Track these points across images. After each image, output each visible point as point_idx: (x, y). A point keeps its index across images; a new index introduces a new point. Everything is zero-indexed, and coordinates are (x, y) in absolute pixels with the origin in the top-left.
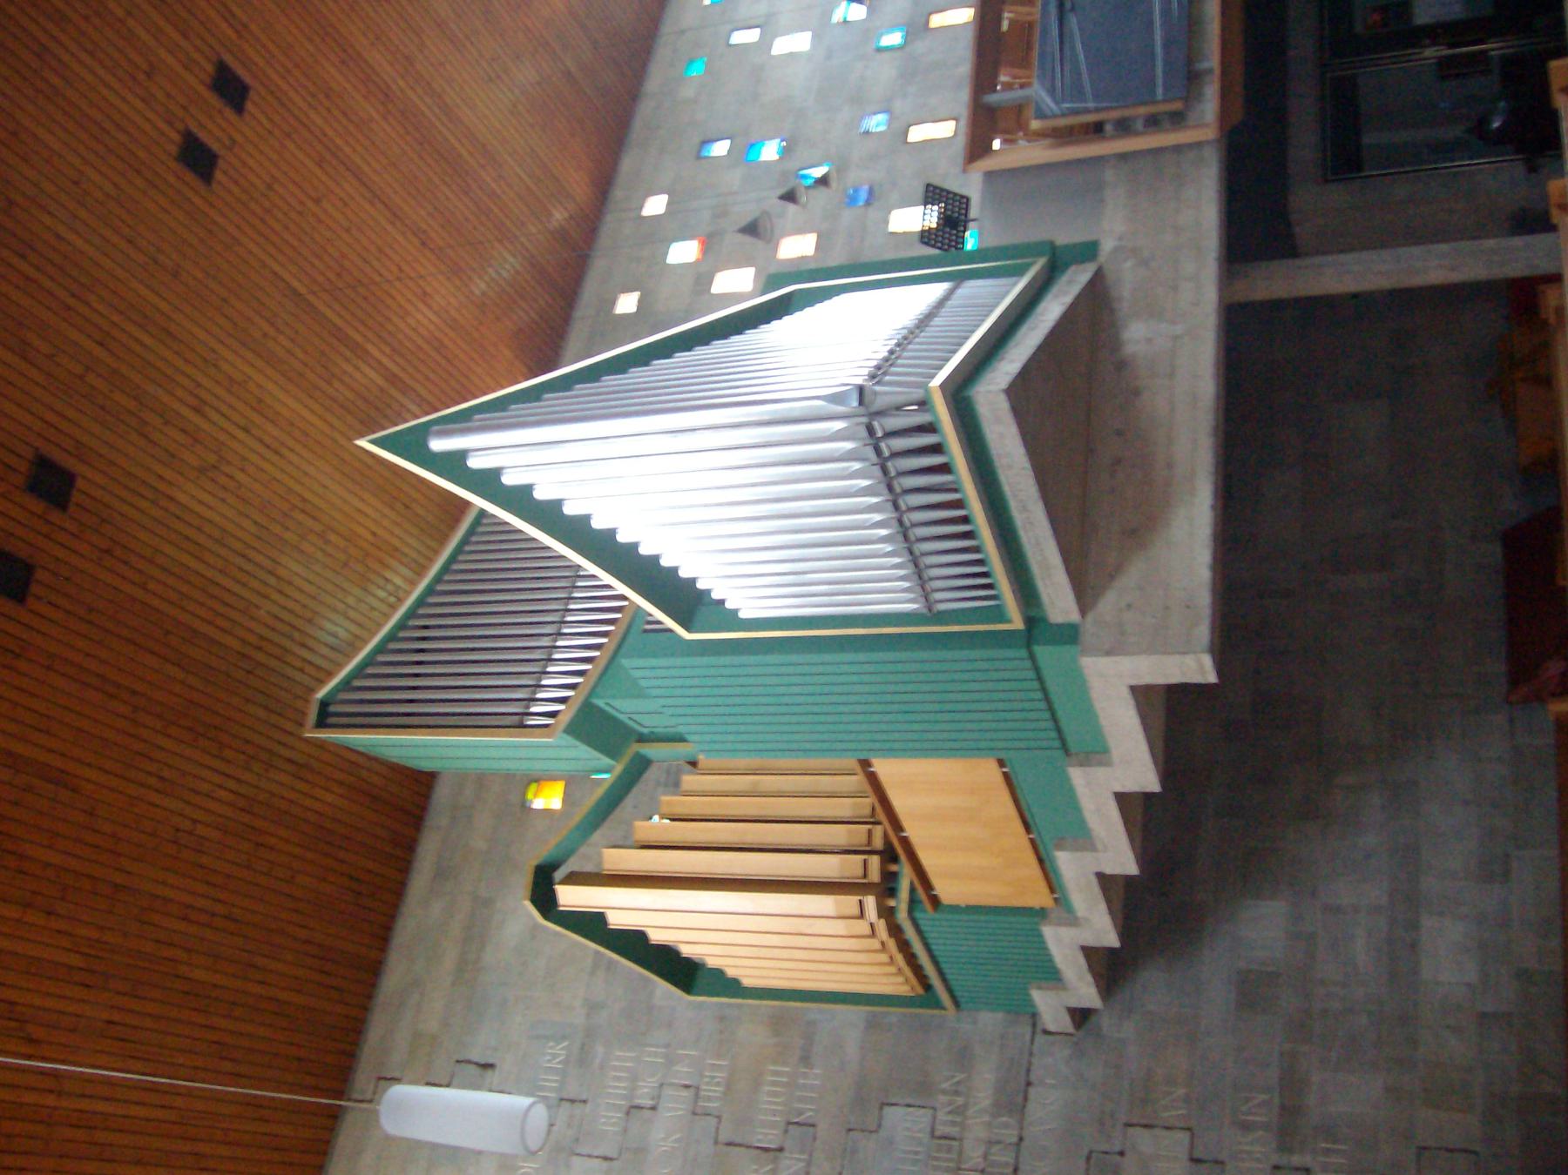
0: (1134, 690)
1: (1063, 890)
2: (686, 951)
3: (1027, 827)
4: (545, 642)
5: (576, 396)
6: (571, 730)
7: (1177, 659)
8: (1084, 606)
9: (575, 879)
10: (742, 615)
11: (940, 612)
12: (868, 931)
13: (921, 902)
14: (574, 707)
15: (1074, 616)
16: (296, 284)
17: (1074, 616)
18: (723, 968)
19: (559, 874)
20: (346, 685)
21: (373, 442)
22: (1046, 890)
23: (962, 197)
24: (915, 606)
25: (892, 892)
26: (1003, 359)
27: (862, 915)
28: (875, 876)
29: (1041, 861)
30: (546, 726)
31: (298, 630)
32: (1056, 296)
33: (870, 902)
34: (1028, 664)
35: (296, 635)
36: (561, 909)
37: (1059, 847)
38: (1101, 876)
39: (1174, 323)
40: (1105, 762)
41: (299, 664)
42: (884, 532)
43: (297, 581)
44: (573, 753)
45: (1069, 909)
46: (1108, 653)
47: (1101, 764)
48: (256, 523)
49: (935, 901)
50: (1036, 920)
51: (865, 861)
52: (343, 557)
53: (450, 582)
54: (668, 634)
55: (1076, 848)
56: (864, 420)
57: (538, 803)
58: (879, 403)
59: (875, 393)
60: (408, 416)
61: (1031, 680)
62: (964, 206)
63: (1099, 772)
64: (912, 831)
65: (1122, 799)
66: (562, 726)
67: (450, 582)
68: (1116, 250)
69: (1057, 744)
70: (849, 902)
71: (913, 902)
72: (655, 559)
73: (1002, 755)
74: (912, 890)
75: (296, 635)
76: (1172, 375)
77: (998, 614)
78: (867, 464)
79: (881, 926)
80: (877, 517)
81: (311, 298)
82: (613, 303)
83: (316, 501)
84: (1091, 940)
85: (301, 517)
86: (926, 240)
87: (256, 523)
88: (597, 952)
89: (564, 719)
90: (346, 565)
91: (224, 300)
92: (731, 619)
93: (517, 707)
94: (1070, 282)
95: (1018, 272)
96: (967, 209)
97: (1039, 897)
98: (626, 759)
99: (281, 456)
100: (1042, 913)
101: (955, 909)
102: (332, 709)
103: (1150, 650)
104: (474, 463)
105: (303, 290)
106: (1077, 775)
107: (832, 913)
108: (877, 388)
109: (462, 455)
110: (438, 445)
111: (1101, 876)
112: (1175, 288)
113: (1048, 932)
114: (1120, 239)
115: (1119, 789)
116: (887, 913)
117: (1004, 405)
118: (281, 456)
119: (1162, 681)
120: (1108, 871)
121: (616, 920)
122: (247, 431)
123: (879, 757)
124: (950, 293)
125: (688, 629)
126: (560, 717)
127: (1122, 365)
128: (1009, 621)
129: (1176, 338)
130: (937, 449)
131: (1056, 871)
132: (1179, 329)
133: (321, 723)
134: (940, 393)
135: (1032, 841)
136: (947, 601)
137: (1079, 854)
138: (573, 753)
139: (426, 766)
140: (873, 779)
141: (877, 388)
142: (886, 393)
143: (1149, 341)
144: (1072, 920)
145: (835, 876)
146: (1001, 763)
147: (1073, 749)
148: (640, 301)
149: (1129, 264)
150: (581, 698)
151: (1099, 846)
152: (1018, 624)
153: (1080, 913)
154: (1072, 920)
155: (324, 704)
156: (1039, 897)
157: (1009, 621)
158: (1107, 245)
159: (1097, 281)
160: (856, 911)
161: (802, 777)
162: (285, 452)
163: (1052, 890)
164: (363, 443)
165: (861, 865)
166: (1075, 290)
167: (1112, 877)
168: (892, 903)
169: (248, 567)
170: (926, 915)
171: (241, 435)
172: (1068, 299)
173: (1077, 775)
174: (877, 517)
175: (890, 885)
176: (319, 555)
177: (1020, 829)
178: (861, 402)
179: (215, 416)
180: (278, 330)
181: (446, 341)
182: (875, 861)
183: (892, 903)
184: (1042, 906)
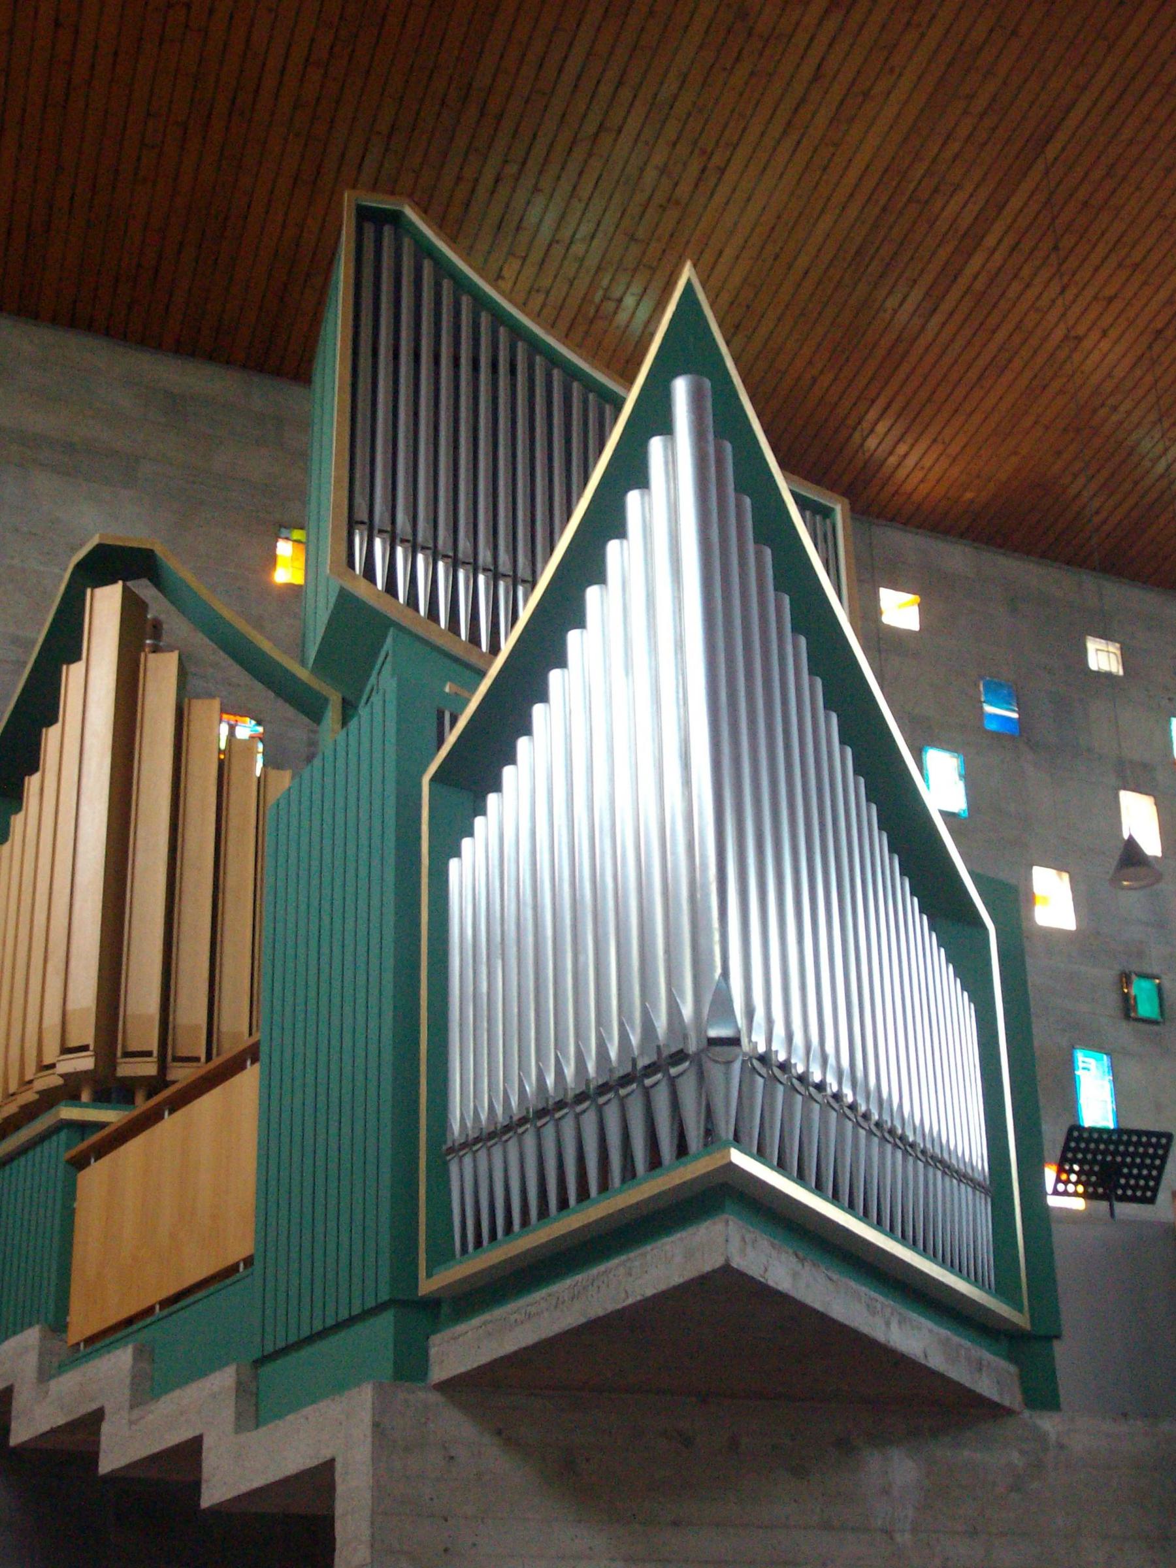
0: (330, 1464)
1: (87, 1357)
2: (33, 783)
3: (167, 1303)
4: (484, 556)
5: (762, 603)
6: (345, 600)
7: (366, 1534)
8: (450, 1387)
9: (132, 610)
10: (453, 863)
11: (446, 1164)
12: (47, 1061)
13: (83, 1140)
14: (382, 604)
15: (438, 1374)
16: (1061, 138)
17: (438, 1374)
18: (10, 839)
19: (144, 589)
20: (425, 250)
21: (689, 284)
22: (88, 1333)
23: (1155, 1190)
24: (456, 1127)
25: (102, 1097)
26: (802, 1261)
27: (66, 1050)
28: (127, 1069)
29: (129, 1321)
30: (351, 564)
31: (521, 171)
32: (945, 1343)
33: (85, 1063)
34: (370, 1303)
35: (513, 169)
36: (89, 591)
37: (138, 1354)
38: (97, 1417)
39: (914, 1530)
40: (240, 1427)
41: (468, 173)
42: (550, 1080)
43: (596, 164)
44: (321, 604)
45: (62, 1368)
46: (376, 1425)
47: (239, 1416)
48: (676, 97)
49: (80, 1163)
50: (50, 1317)
51: (149, 1054)
52: (641, 234)
53: (585, 401)
54: (435, 744)
55: (137, 1378)
56: (692, 1048)
57: (284, 549)
58: (715, 1072)
59: (729, 1063)
60: (739, 340)
61: (363, 1304)
62: (1129, 1193)
63: (228, 1413)
64: (170, 1123)
65: (192, 1449)
66: (348, 586)
67: (585, 401)
68: (1042, 1438)
69: (269, 1348)
70: (84, 1032)
71: (84, 1128)
72: (526, 729)
73: (258, 1262)
74: (102, 1125)
75: (513, 169)
76: (827, 1526)
77: (441, 1255)
78: (636, 1052)
79: (52, 1080)
80: (569, 1071)
81: (1040, 166)
82: (1105, 636)
83: (724, 190)
84: (20, 1402)
85: (694, 168)
86: (1076, 1134)
87: (676, 97)
88: (33, 643)
89: (361, 589)
90: (633, 238)
91: (1014, 33)
92: (447, 848)
93: (382, 514)
94: (980, 1366)
95: (1004, 1287)
96: (1133, 1199)
97: (82, 1323)
98: (316, 684)
99: (785, 133)
100: (58, 1326)
101: (70, 1193)
102: (387, 230)
103: (379, 1489)
104: (656, 445)
105: (1051, 151)
106: (224, 1379)
107: (70, 1006)
108: (737, 1066)
109: (666, 428)
110: (681, 388)
111: (97, 1417)
112: (974, 1533)
113: (32, 1336)
114: (1061, 1446)
115: (207, 1443)
116: (70, 1089)
117: (710, 1263)
118: (785, 133)
119: (340, 1507)
120: (105, 1428)
121: (73, 674)
122: (817, 76)
123: (261, 1073)
124: (962, 1177)
125: (433, 780)
126: (364, 582)
127: (845, 1446)
128: (429, 1275)
129: (889, 1533)
130: (655, 1162)
131: (109, 1348)
132: (904, 1538)
133: (364, 215)
134: (1046, 1154)
135: (149, 1311)
136: (461, 1173)
137: (128, 1381)
138: (321, 604)
139: (317, 380)
140: (234, 1066)
141: (737, 1066)
142: (728, 1080)
143: (886, 1491)
144: (45, 1375)
145: (129, 1009)
146: (249, 1261)
147: (267, 1370)
148: (1108, 675)
149: (1016, 1458)
150: (394, 616)
151: (136, 1413)
152: (427, 1286)
153: (55, 1386)
154: (45, 1375)
155: (395, 218)
156: (82, 1323)
157: (429, 1275)
158: (1049, 1424)
159: (995, 1411)
160: (73, 1043)
161: (249, 954)
162: (788, 144)
163: (91, 1340)
164: (687, 273)
165: (145, 1048)
166: (959, 1373)
167: (97, 1432)
168: (85, 1096)
169: (605, 90)
170: (60, 1149)
171: (807, 71)
172: (936, 1362)
173: (224, 1379)
174: (569, 1071)
175: (114, 1096)
176: (640, 198)
177: (164, 1294)
178: (713, 1042)
179: (831, 25)
180: (982, 116)
181: (1009, 375)
182: (148, 1068)
183: (85, 1096)
184: (70, 1326)
